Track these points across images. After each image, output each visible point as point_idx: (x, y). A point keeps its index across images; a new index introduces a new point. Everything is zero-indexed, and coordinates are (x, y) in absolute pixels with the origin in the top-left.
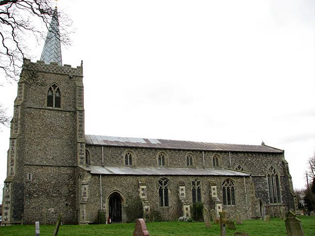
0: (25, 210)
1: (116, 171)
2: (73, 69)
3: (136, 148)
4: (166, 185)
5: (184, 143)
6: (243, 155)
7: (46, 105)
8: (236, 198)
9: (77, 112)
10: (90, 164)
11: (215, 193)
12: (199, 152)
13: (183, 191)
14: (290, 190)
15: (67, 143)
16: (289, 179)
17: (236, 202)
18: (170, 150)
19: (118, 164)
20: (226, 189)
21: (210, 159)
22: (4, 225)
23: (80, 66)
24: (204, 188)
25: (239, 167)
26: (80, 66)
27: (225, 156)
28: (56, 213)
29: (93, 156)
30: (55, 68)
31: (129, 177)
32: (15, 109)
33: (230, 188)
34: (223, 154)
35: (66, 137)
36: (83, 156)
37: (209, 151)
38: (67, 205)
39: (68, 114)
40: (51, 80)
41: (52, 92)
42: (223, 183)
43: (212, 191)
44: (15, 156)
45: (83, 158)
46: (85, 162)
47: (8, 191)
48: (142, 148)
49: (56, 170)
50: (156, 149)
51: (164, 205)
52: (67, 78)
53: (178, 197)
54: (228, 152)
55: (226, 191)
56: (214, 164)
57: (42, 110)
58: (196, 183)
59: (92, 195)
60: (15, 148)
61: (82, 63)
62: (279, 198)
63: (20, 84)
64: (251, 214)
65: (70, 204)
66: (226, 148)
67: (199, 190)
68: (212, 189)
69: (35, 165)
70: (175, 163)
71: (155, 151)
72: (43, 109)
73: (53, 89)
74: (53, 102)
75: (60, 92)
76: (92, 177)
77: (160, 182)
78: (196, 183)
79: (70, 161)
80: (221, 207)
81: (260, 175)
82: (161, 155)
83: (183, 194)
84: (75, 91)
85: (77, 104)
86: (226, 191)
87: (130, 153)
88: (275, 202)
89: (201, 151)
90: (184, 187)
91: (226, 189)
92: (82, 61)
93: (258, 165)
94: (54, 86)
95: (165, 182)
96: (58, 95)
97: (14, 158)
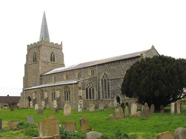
5: (107, 59)
33: (68, 91)
43: (57, 93)
51: (104, 98)
61: (62, 43)
70: (71, 77)
81: (119, 78)
92: (62, 42)
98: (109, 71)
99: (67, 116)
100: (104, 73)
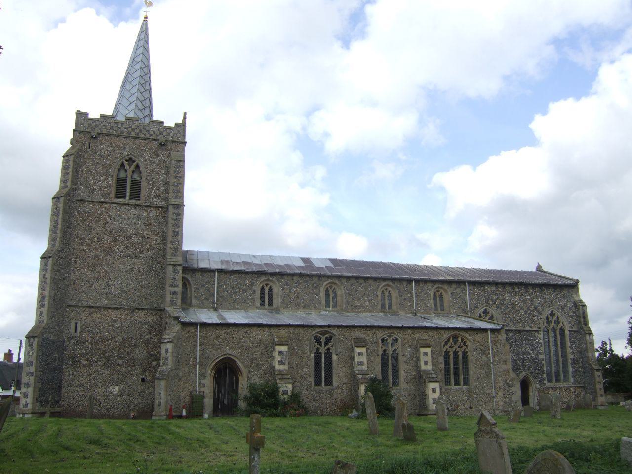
0: (63, 389)
1: (234, 317)
2: (166, 128)
3: (282, 275)
4: (330, 345)
6: (494, 288)
7: (112, 195)
8: (471, 373)
9: (171, 208)
10: (190, 305)
11: (427, 360)
12: (405, 283)
13: (361, 356)
14: (588, 357)
15: (149, 265)
16: (588, 337)
17: (471, 380)
18: (348, 278)
19: (243, 304)
20: (451, 353)
21: (427, 295)
22: (21, 416)
23: (180, 122)
24: (404, 353)
25: (486, 312)
26: (180, 122)
27: (458, 290)
28: (121, 395)
29: (197, 289)
30: (134, 127)
31: (211, 328)
32: (54, 204)
33: (460, 353)
34: (454, 286)
35: (147, 254)
36: (176, 289)
37: (425, 282)
38: (143, 380)
39: (154, 212)
40: (127, 148)
41: (126, 171)
42: (446, 343)
44: (48, 289)
45: (175, 293)
46: (179, 302)
47: (31, 353)
48: (293, 275)
49: (125, 315)
50: (320, 277)
52: (155, 145)
53: (351, 367)
54: (464, 283)
55: (451, 357)
56: (435, 305)
57: (105, 205)
58: (390, 341)
59: (178, 363)
60: (48, 276)
61: (185, 118)
62: (566, 372)
63: (66, 158)
64: (501, 403)
65: (148, 378)
66: (463, 275)
67: (396, 358)
68: (422, 354)
69: (87, 307)
70: (356, 302)
71: (319, 280)
72: (107, 203)
73: (127, 167)
74: (125, 191)
75: (141, 173)
76: (182, 328)
77: (318, 340)
78: (390, 341)
79: (153, 300)
80: (438, 390)
81: (528, 328)
82: (331, 287)
83: (361, 363)
84: (168, 170)
85: (171, 194)
86: (451, 357)
87: (271, 284)
88: (558, 380)
89: (409, 281)
90: (364, 350)
91: (451, 353)
92: (185, 114)
93: (525, 309)
94: (130, 161)
95: (326, 338)
96: (136, 177)
97: (47, 294)
98: (498, 307)
99: (155, 470)
100: (483, 310)
